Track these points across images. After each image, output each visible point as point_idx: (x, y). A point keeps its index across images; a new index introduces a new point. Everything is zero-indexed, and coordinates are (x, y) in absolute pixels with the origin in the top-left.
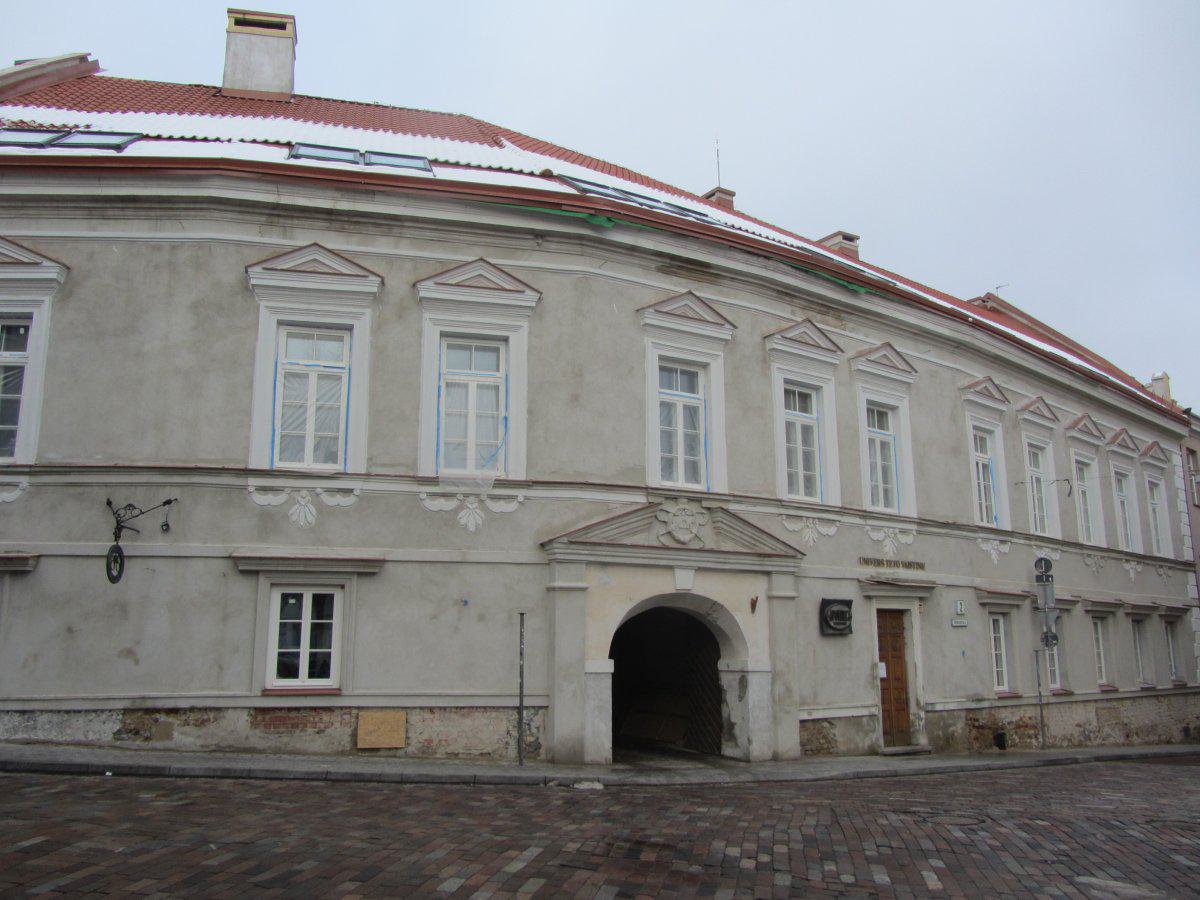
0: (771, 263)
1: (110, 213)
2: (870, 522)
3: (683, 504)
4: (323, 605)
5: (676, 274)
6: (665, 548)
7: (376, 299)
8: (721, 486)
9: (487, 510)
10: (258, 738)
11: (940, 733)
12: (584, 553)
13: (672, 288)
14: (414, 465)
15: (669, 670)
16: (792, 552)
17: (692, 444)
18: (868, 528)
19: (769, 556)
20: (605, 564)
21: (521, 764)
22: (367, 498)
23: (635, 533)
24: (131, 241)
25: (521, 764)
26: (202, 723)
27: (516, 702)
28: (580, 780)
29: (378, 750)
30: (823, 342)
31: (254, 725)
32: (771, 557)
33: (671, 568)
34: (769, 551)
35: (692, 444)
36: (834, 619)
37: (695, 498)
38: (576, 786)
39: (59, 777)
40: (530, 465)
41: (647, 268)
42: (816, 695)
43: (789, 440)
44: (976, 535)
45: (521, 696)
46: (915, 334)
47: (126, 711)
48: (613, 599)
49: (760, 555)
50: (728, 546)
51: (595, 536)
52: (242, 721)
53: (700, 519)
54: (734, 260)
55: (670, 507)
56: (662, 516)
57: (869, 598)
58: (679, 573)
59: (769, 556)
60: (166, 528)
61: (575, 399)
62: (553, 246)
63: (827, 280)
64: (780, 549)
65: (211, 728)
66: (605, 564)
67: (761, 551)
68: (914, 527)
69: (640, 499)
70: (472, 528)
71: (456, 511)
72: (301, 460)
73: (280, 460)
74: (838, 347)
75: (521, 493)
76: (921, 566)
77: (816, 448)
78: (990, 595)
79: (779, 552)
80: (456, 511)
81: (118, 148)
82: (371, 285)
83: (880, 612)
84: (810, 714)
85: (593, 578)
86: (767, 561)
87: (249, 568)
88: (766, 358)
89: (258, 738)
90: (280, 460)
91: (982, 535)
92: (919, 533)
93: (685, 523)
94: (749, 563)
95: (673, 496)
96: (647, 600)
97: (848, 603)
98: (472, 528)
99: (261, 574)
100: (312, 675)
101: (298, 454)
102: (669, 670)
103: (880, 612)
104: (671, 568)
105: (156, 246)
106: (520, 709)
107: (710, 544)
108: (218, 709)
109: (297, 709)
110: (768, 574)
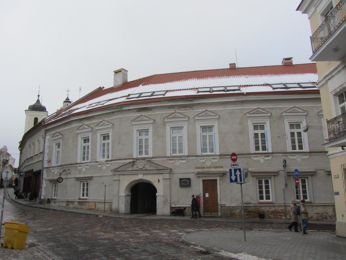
0: (161, 102)
1: (66, 125)
2: (199, 158)
3: (140, 160)
4: (267, 182)
5: (141, 111)
6: (137, 170)
7: (91, 131)
8: (150, 155)
9: (106, 166)
10: (79, 206)
11: (228, 212)
12: (118, 173)
13: (79, 125)
14: (132, 155)
15: (142, 196)
16: (167, 168)
17: (104, 151)
18: (199, 159)
19: (161, 170)
20: (124, 175)
21: (104, 212)
22: (91, 166)
23: (129, 168)
24: (68, 129)
25: (104, 212)
26: (73, 204)
27: (104, 201)
28: (100, 215)
29: (92, 209)
30: (182, 116)
31: (78, 204)
32: (160, 170)
33: (137, 174)
34: (161, 168)
35: (104, 151)
36: (185, 183)
37: (143, 159)
38: (99, 216)
39: (72, 211)
40: (189, 151)
41: (135, 112)
42: (178, 201)
43: (88, 151)
44: (251, 156)
45: (105, 200)
46: (222, 103)
47: (67, 202)
48: (126, 181)
49: (158, 170)
50: (152, 168)
51: (120, 169)
52: (76, 203)
53: (146, 163)
54: (153, 104)
55: (138, 162)
56: (137, 164)
57: (199, 177)
58: (139, 175)
59: (161, 170)
60: (70, 173)
61: (119, 143)
62: (116, 114)
63: (180, 101)
64: (164, 168)
65: (74, 205)
66: (124, 175)
67: (159, 169)
68: (219, 157)
69: (131, 161)
70: (104, 170)
71: (102, 167)
72: (142, 155)
73: (173, 154)
74: (185, 116)
75: (110, 162)
76: (222, 167)
77: (82, 151)
78: (251, 173)
79: (164, 169)
80: (102, 167)
81: (164, 95)
82: (90, 129)
83: (203, 180)
84: (176, 206)
85: (121, 178)
86: (160, 171)
87: (78, 179)
88: (164, 124)
89: (79, 206)
90: (173, 154)
91: (253, 156)
92: (220, 158)
93: (140, 165)
94: (155, 172)
95: (138, 159)
96: (148, 181)
97: (189, 179)
98: (262, 163)
99: (291, 176)
100: (266, 199)
101: (206, 152)
102: (142, 196)
103: (203, 180)
104: (137, 174)
105: (69, 129)
106: (105, 202)
107: (148, 169)
108: (75, 202)
109: (82, 202)
110: (162, 173)
